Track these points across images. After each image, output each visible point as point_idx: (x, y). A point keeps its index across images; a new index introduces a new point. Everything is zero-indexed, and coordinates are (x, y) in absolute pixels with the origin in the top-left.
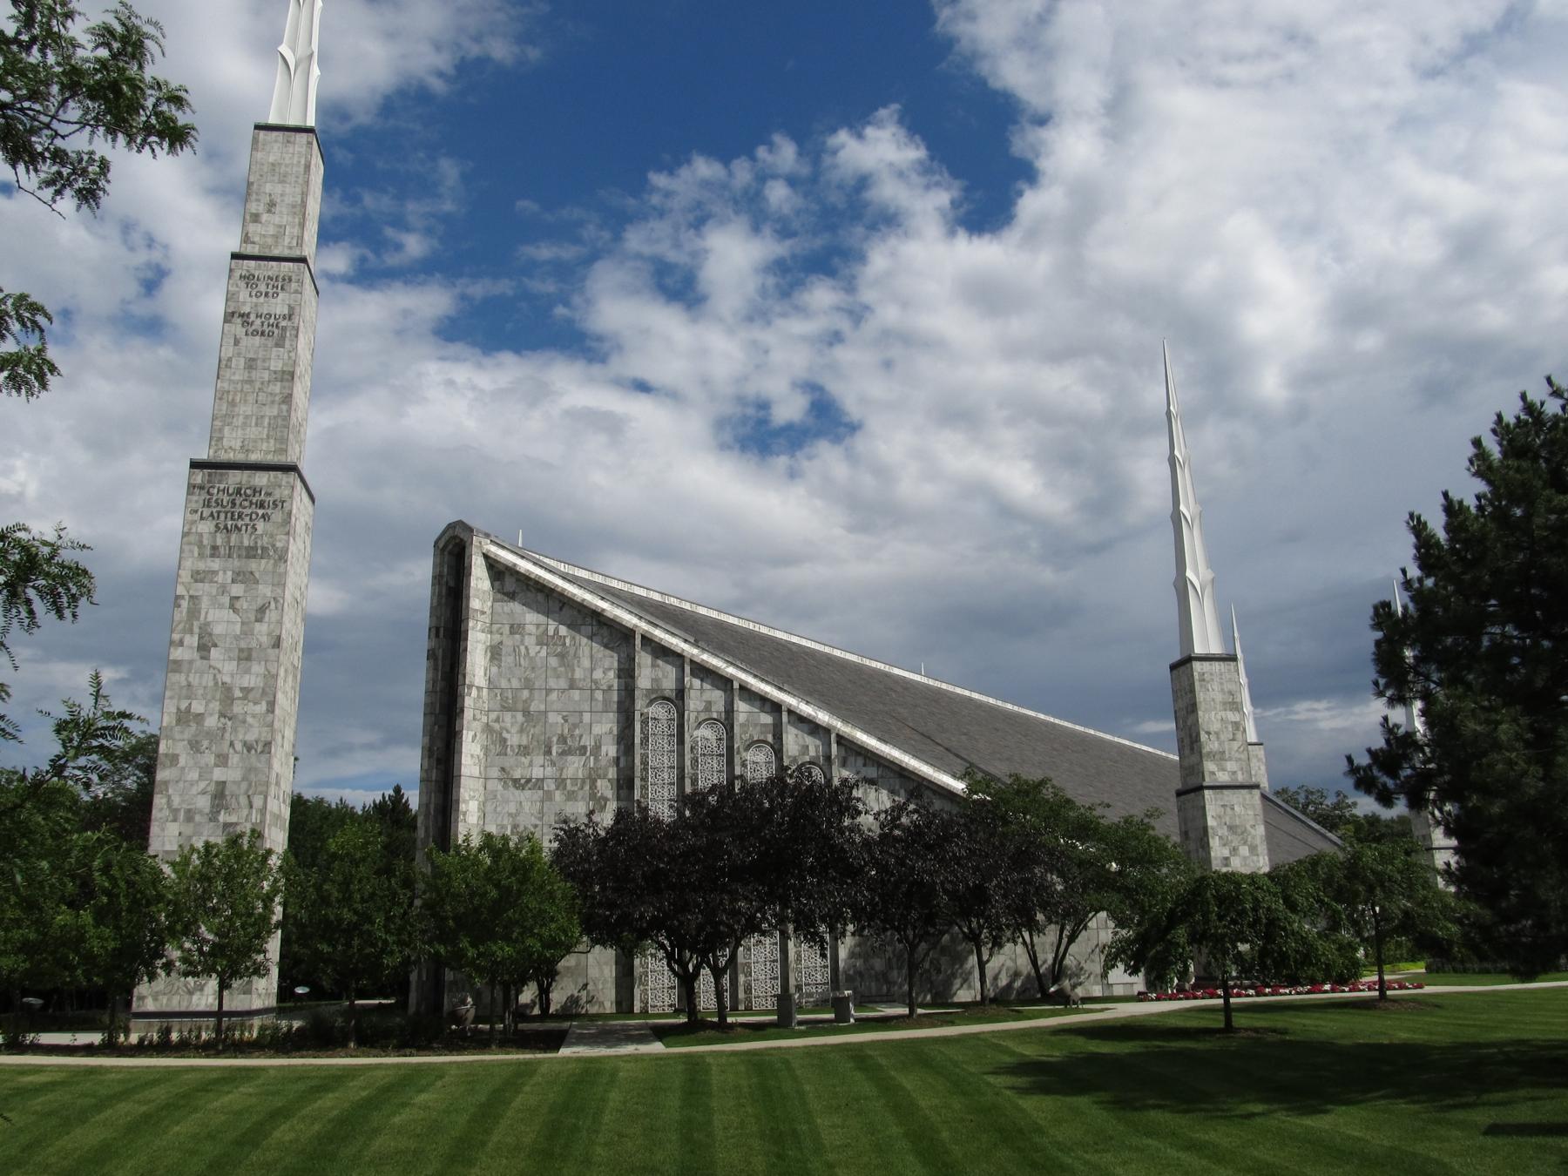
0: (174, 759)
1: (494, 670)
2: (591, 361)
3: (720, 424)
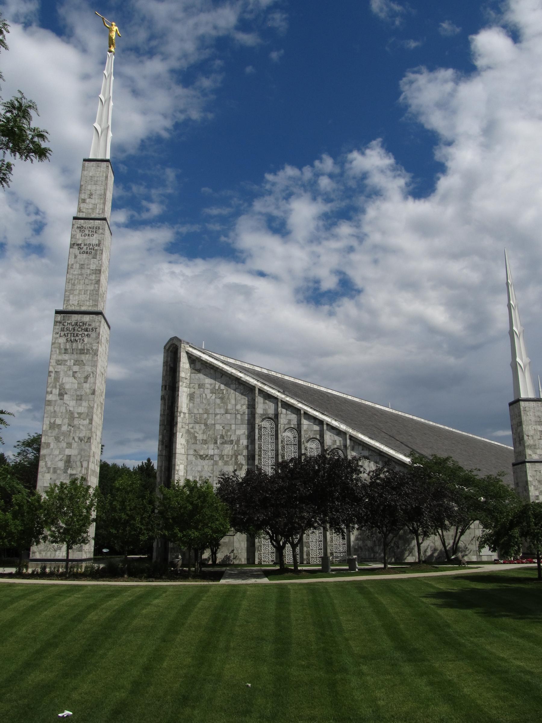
0: (48, 445)
1: (191, 405)
2: (237, 262)
3: (297, 291)
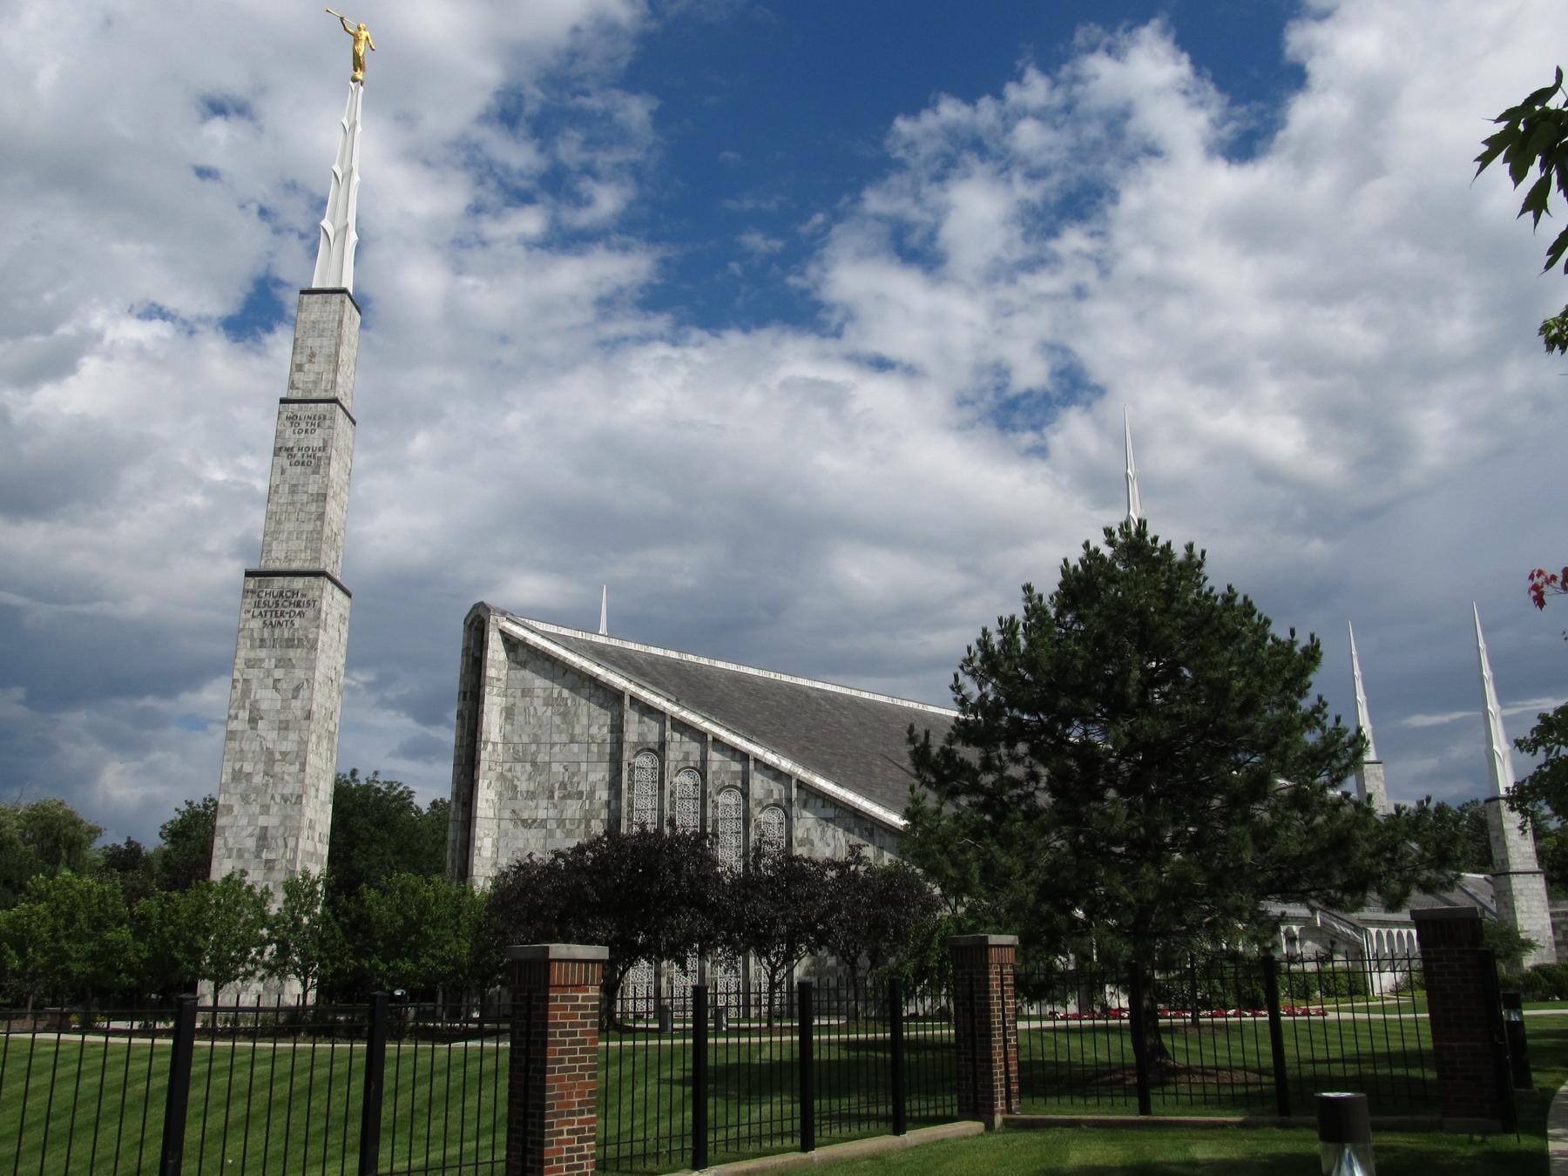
0: (230, 809)
1: (508, 727)
3: (962, 401)
